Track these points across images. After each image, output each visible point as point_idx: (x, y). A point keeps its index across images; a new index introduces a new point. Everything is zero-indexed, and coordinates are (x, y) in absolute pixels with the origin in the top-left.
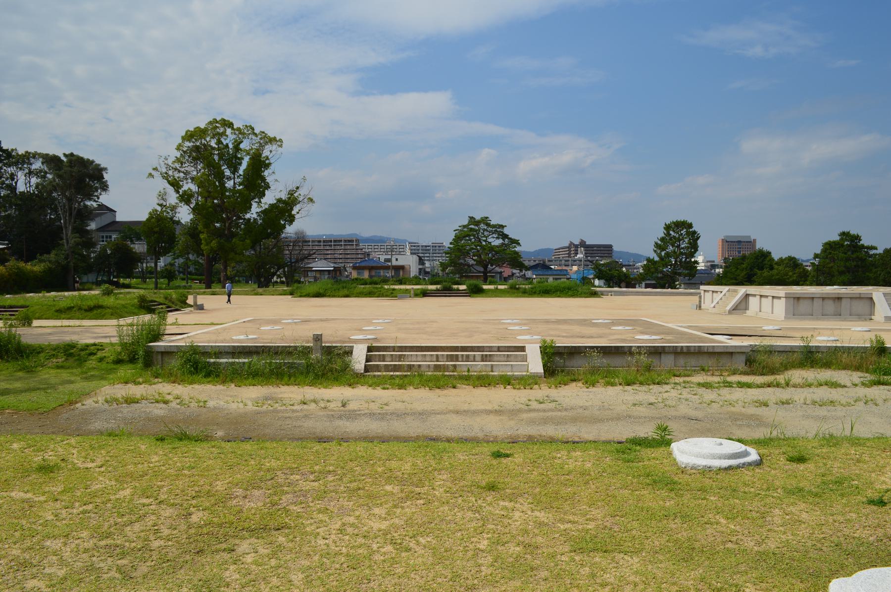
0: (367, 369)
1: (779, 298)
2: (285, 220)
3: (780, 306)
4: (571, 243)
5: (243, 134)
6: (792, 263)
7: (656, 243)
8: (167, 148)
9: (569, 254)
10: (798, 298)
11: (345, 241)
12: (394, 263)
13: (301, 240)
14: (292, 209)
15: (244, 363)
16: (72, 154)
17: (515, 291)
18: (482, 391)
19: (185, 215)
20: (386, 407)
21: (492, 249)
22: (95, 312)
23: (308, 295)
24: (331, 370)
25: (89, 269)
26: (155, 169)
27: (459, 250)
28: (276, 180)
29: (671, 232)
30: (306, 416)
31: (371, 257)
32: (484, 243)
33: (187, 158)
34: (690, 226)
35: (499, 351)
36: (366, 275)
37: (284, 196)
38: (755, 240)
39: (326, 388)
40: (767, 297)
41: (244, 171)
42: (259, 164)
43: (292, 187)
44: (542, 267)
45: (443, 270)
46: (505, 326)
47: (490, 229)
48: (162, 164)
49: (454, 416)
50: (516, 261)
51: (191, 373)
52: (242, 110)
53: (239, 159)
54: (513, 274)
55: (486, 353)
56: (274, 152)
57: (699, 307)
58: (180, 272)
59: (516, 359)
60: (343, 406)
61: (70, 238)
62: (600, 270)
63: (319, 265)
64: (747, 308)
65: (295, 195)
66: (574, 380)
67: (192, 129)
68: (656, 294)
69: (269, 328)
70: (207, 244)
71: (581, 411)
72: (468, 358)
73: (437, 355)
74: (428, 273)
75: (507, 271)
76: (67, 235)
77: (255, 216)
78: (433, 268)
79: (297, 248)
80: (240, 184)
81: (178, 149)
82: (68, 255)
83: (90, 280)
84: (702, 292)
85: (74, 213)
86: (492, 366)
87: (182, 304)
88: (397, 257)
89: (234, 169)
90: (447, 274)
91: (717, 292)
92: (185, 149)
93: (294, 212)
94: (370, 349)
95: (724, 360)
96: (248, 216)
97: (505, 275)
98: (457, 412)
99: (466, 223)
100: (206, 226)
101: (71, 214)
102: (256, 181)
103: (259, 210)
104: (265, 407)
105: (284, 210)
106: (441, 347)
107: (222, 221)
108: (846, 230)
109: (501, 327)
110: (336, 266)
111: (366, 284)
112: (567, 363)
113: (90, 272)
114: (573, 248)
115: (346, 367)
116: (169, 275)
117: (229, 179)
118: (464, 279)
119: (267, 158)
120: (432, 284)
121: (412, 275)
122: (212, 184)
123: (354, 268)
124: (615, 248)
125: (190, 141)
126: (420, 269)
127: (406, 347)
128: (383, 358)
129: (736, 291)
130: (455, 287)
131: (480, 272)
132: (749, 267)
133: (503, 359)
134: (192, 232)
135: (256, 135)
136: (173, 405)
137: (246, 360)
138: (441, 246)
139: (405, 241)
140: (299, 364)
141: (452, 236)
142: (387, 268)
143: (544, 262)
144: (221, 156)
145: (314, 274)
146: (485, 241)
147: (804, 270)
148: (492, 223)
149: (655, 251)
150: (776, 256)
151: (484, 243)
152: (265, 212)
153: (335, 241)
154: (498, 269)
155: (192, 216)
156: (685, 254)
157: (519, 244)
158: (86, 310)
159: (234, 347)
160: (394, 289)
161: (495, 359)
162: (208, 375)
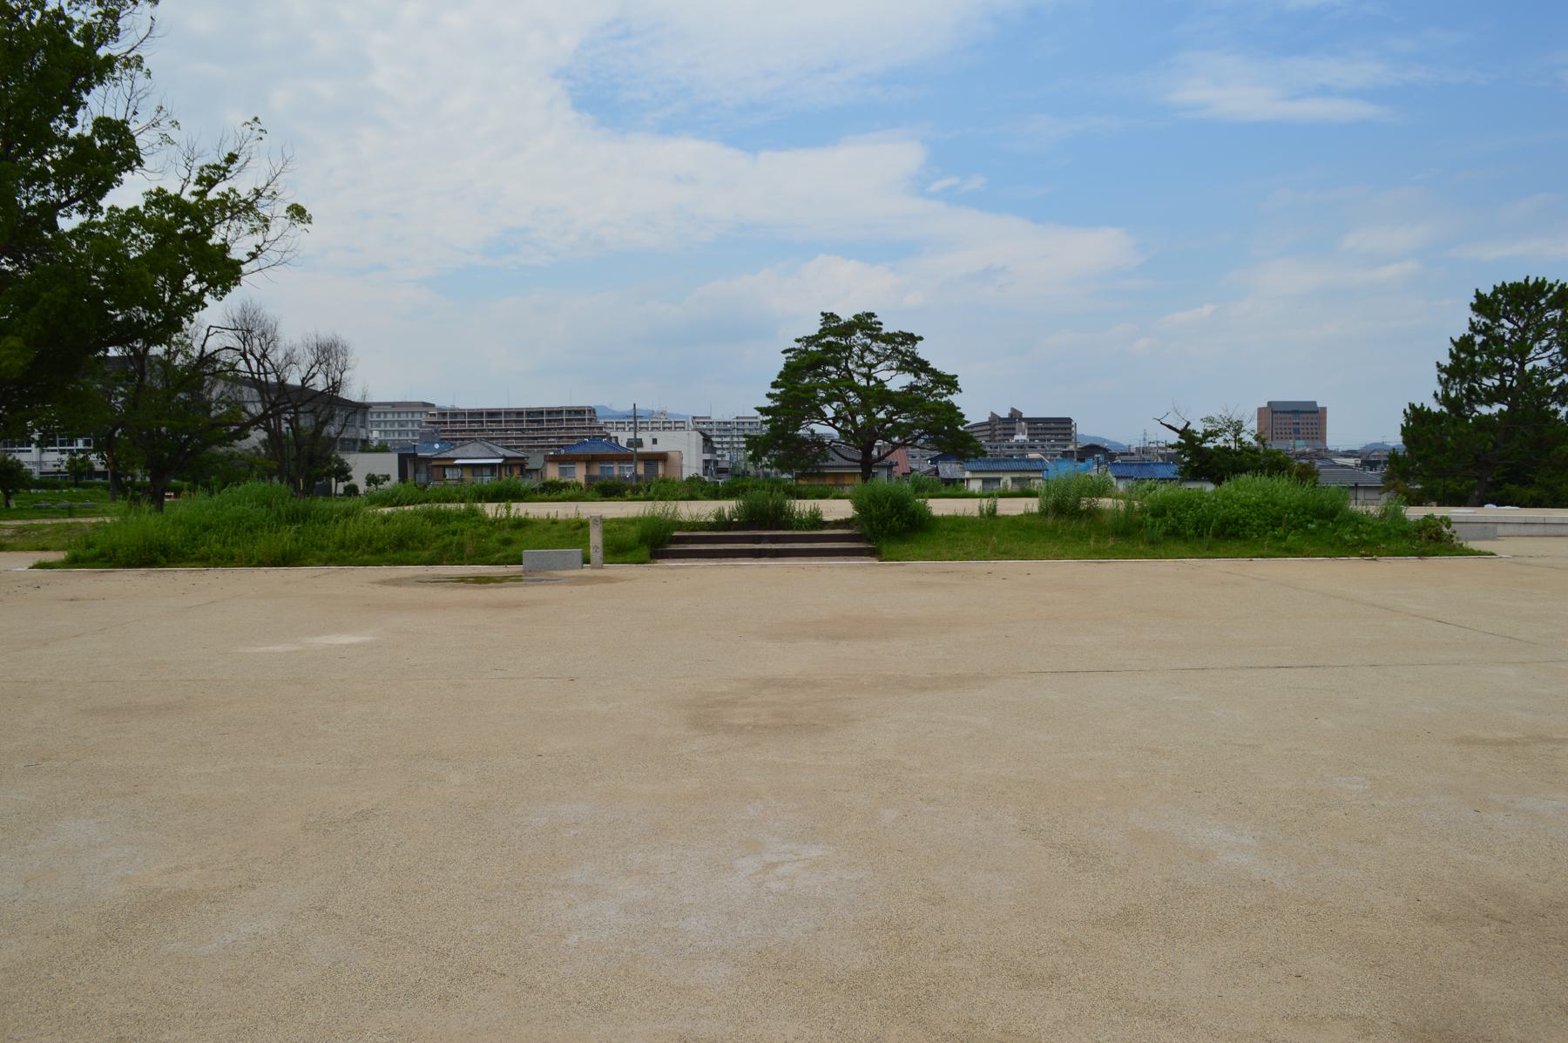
12: (648, 447)
36: (579, 474)
38: (1324, 409)
88: (656, 434)
110: (509, 453)
126: (706, 461)
130: (802, 506)
145: (457, 473)
146: (868, 377)
151: (864, 383)
160: (521, 524)
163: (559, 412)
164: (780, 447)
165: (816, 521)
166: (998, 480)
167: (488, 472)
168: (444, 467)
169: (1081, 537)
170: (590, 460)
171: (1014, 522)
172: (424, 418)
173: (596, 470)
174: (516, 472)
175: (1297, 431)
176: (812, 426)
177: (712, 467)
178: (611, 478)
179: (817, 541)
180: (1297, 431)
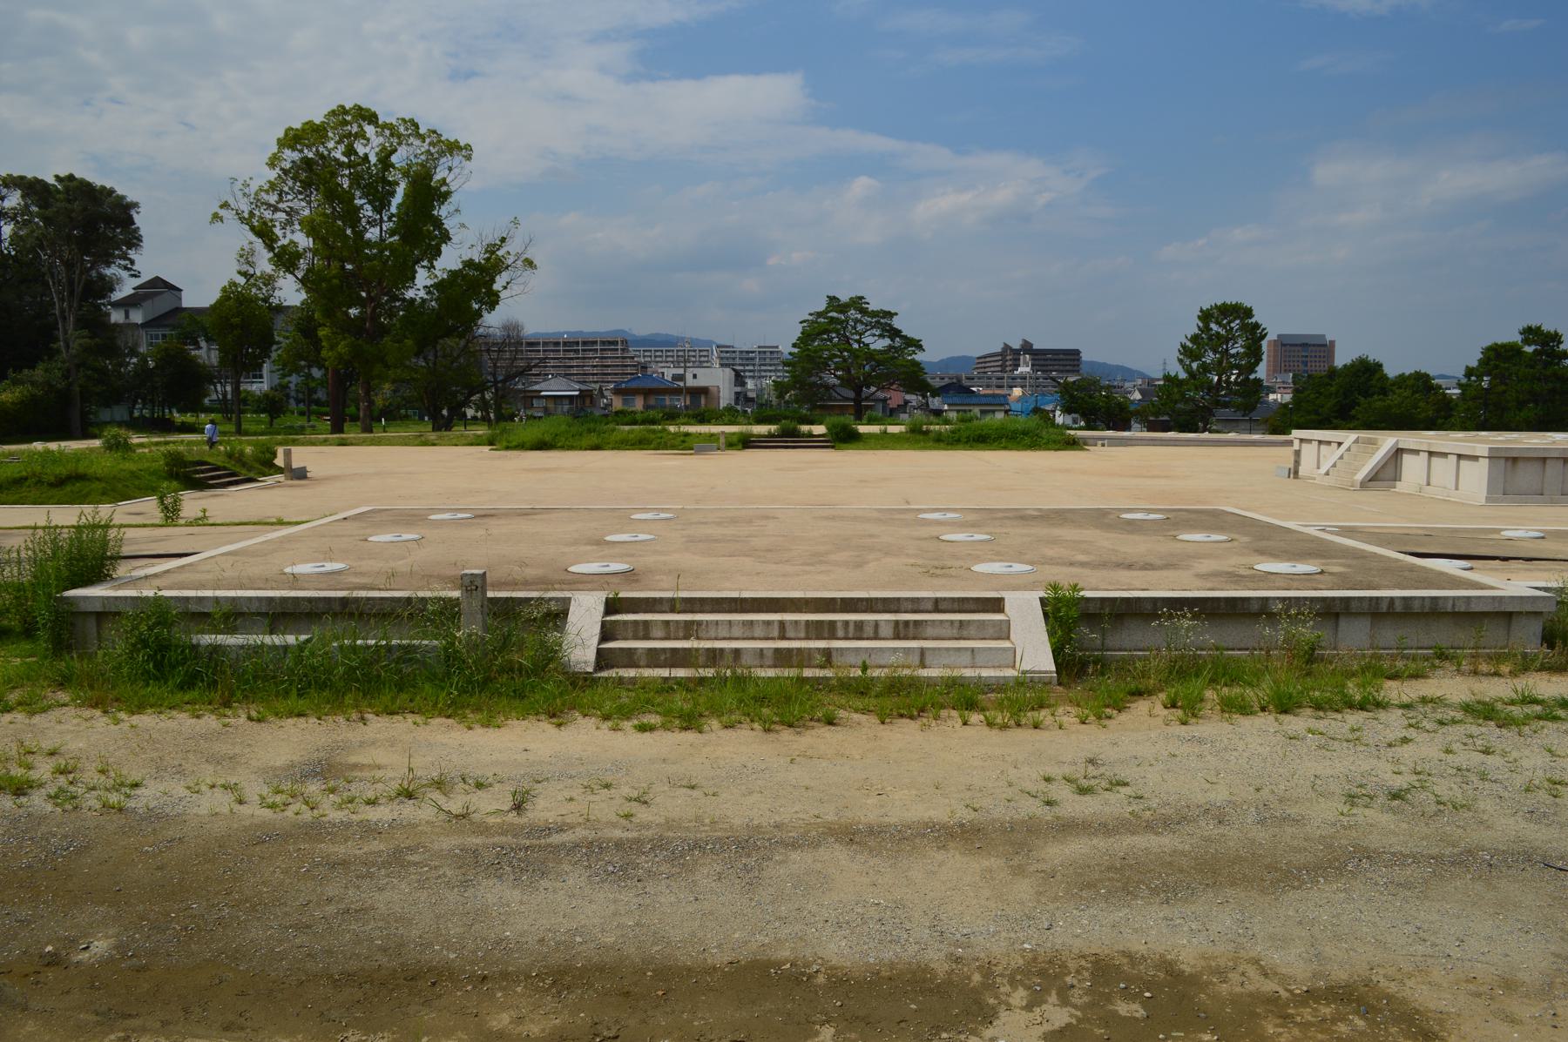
0: (604, 659)
1: (1475, 458)
2: (481, 302)
3: (1476, 477)
4: (1006, 347)
5: (399, 136)
6: (1421, 383)
7: (1184, 346)
8: (251, 162)
9: (1003, 367)
10: (1515, 460)
11: (603, 343)
12: (690, 382)
13: (513, 341)
14: (493, 281)
15: (286, 648)
16: (71, 177)
17: (919, 437)
18: (905, 735)
19: (290, 292)
20: (643, 814)
21: (871, 355)
22: (68, 488)
23: (521, 447)
24: (509, 669)
25: (112, 397)
26: (225, 205)
27: (810, 359)
28: (463, 226)
29: (1213, 326)
30: (397, 860)
31: (649, 371)
32: (856, 346)
33: (290, 183)
34: (1248, 313)
35: (937, 610)
36: (638, 404)
37: (477, 256)
38: (1332, 343)
39: (486, 725)
40: (1445, 455)
41: (399, 206)
42: (427, 193)
43: (492, 237)
44: (957, 389)
45: (781, 396)
46: (934, 531)
47: (867, 319)
48: (240, 194)
49: (837, 856)
50: (914, 379)
51: (147, 677)
52: (404, 90)
53: (390, 184)
54: (907, 402)
55: (904, 616)
56: (456, 171)
57: (1295, 473)
58: (298, 401)
59: (983, 631)
60: (518, 808)
61: (71, 340)
62: (1072, 396)
63: (555, 387)
64: (1397, 477)
65: (500, 253)
66: (1138, 694)
67: (298, 125)
68: (1188, 443)
69: (388, 537)
70: (332, 348)
71: (1209, 828)
72: (859, 631)
73: (782, 624)
74: (752, 400)
75: (896, 397)
76: (66, 332)
77: (422, 294)
78: (760, 391)
79: (507, 355)
80: (392, 233)
81: (272, 164)
82: (68, 371)
83: (118, 418)
84: (1296, 443)
85: (79, 289)
86: (923, 651)
87: (265, 465)
88: (696, 371)
89: (381, 203)
90: (787, 402)
91: (1329, 443)
92: (288, 166)
93: (496, 287)
94: (612, 606)
95: (1493, 635)
96: (410, 294)
97: (893, 404)
98: (851, 836)
99: (822, 307)
100: (329, 313)
101: (71, 293)
102: (422, 227)
103: (429, 282)
104: (289, 813)
105: (478, 283)
106: (792, 600)
107: (360, 302)
108: (1534, 323)
109: (925, 532)
110: (584, 387)
111: (634, 423)
112: (1110, 642)
113: (117, 402)
114: (1009, 356)
115: (549, 660)
116: (272, 406)
117: (372, 223)
118: (817, 412)
119: (444, 182)
120: (760, 421)
121: (723, 404)
122: (336, 232)
123: (617, 392)
124: (1085, 357)
125: (294, 149)
127: (702, 600)
128: (644, 631)
129: (1372, 442)
130: (805, 428)
131: (847, 399)
132: (1351, 396)
133: (948, 632)
134: (306, 324)
135: (422, 138)
136: (37, 801)
137: (291, 639)
138: (774, 351)
139: (710, 343)
140: (427, 650)
141: (796, 332)
142: (677, 392)
143: (959, 380)
144: (356, 180)
145: (543, 403)
146: (859, 342)
147: (1445, 395)
148: (871, 308)
149: (1180, 361)
150: (1391, 371)
151: (856, 346)
152: (440, 286)
153: (585, 343)
154: (881, 395)
155: (303, 296)
156: (1237, 366)
157: (920, 347)
158: (51, 485)
159: (270, 599)
160: (687, 434)
161: (930, 631)
162: (188, 684)
165: (810, 435)
169: (918, 442)
171: (893, 435)
179: (811, 442)
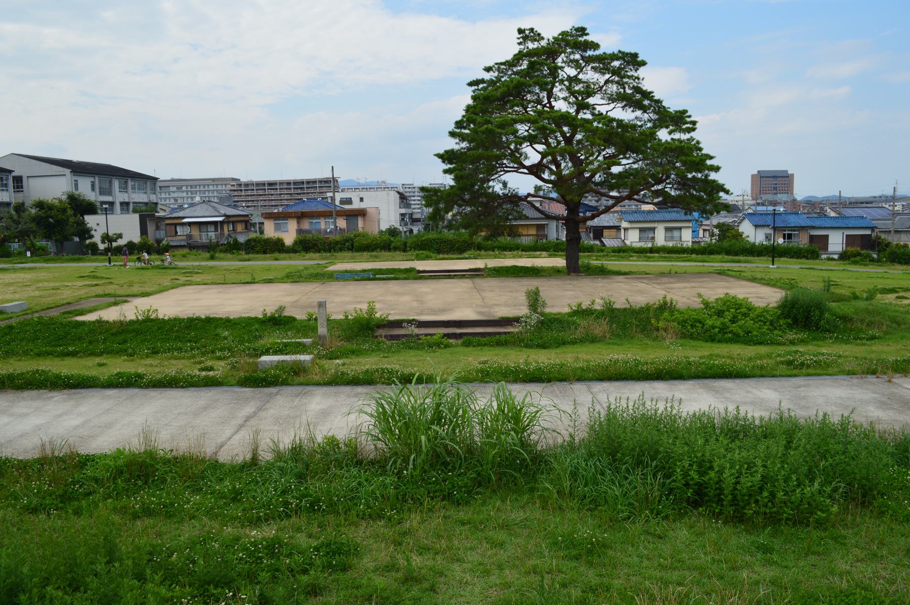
12: (356, 205)
38: (792, 175)
88: (362, 194)
110: (231, 212)
126: (402, 215)
145: (187, 230)
163: (314, 182)
164: (467, 203)
166: (653, 229)
167: (212, 228)
168: (176, 225)
170: (300, 217)
172: (229, 187)
173: (306, 225)
174: (240, 227)
175: (775, 189)
176: (506, 177)
177: (407, 219)
178: (319, 231)
180: (775, 189)
